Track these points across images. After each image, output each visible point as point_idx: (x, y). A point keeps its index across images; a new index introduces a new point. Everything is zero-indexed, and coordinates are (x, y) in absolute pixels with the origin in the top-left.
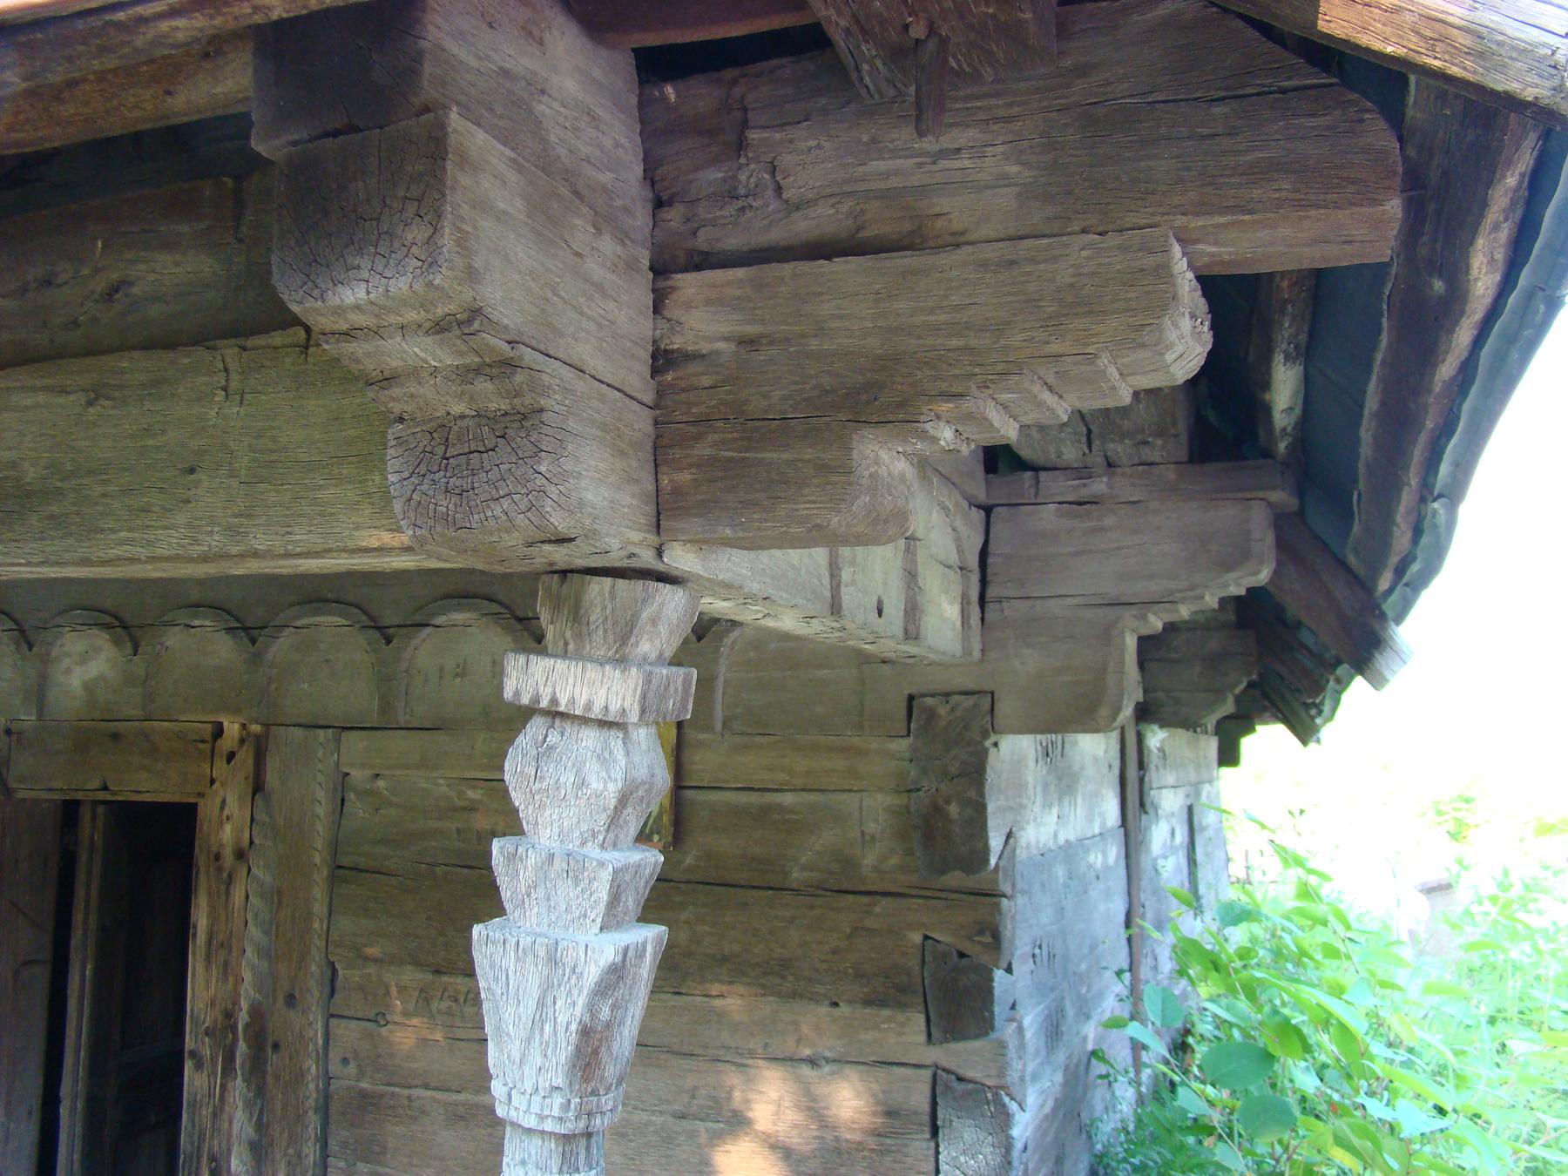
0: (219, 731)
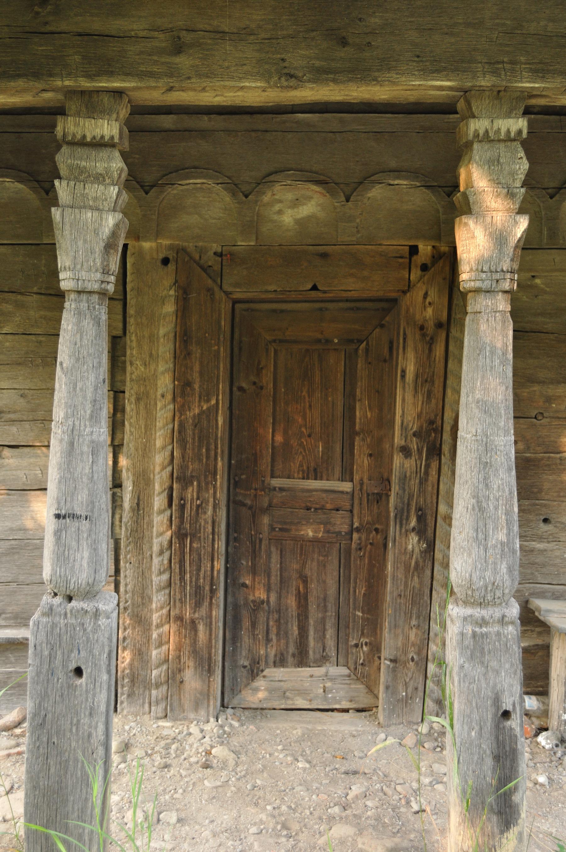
0: (414, 250)
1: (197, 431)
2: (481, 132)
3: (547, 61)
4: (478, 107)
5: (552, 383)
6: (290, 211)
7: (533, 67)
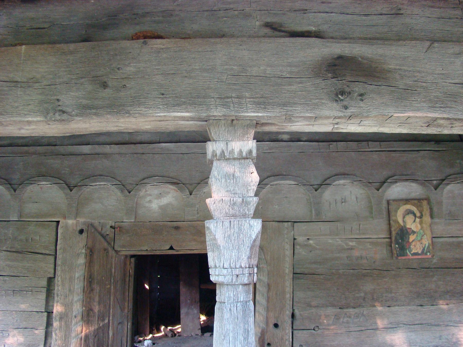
1: (96, 340)
2: (218, 153)
3: (267, 95)
4: (216, 133)
5: (323, 307)
6: (156, 201)
7: (256, 100)
